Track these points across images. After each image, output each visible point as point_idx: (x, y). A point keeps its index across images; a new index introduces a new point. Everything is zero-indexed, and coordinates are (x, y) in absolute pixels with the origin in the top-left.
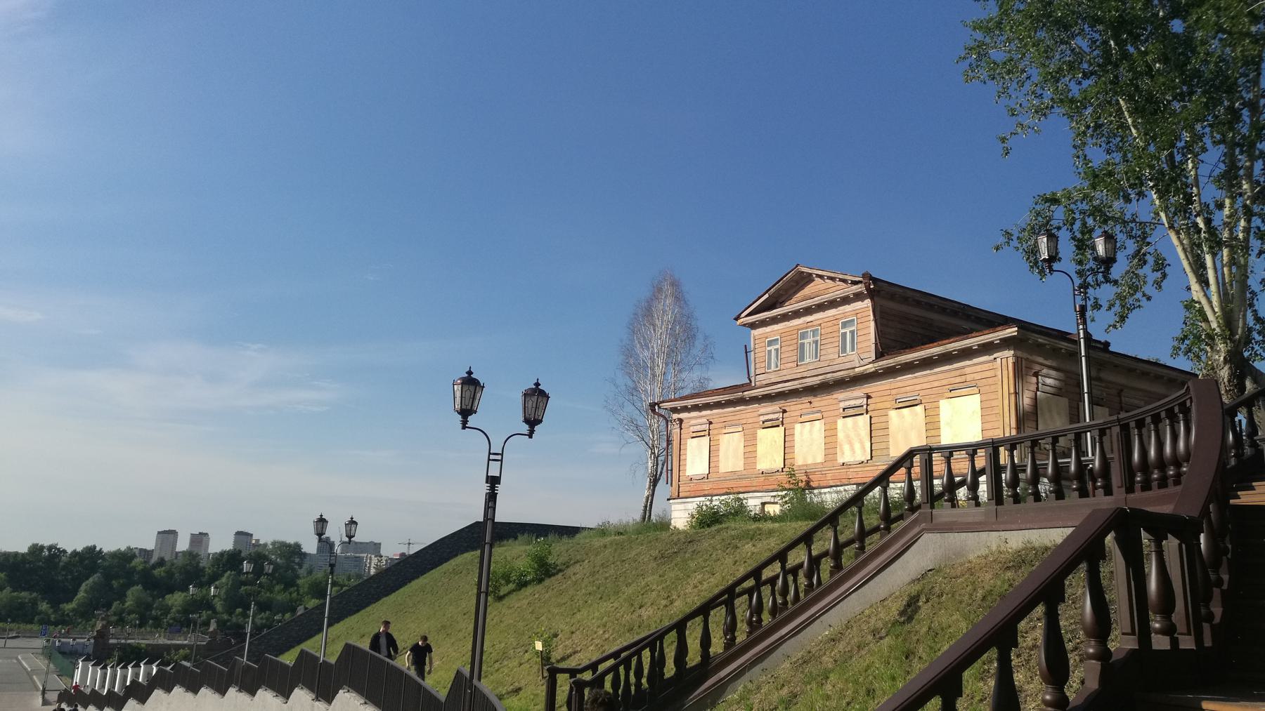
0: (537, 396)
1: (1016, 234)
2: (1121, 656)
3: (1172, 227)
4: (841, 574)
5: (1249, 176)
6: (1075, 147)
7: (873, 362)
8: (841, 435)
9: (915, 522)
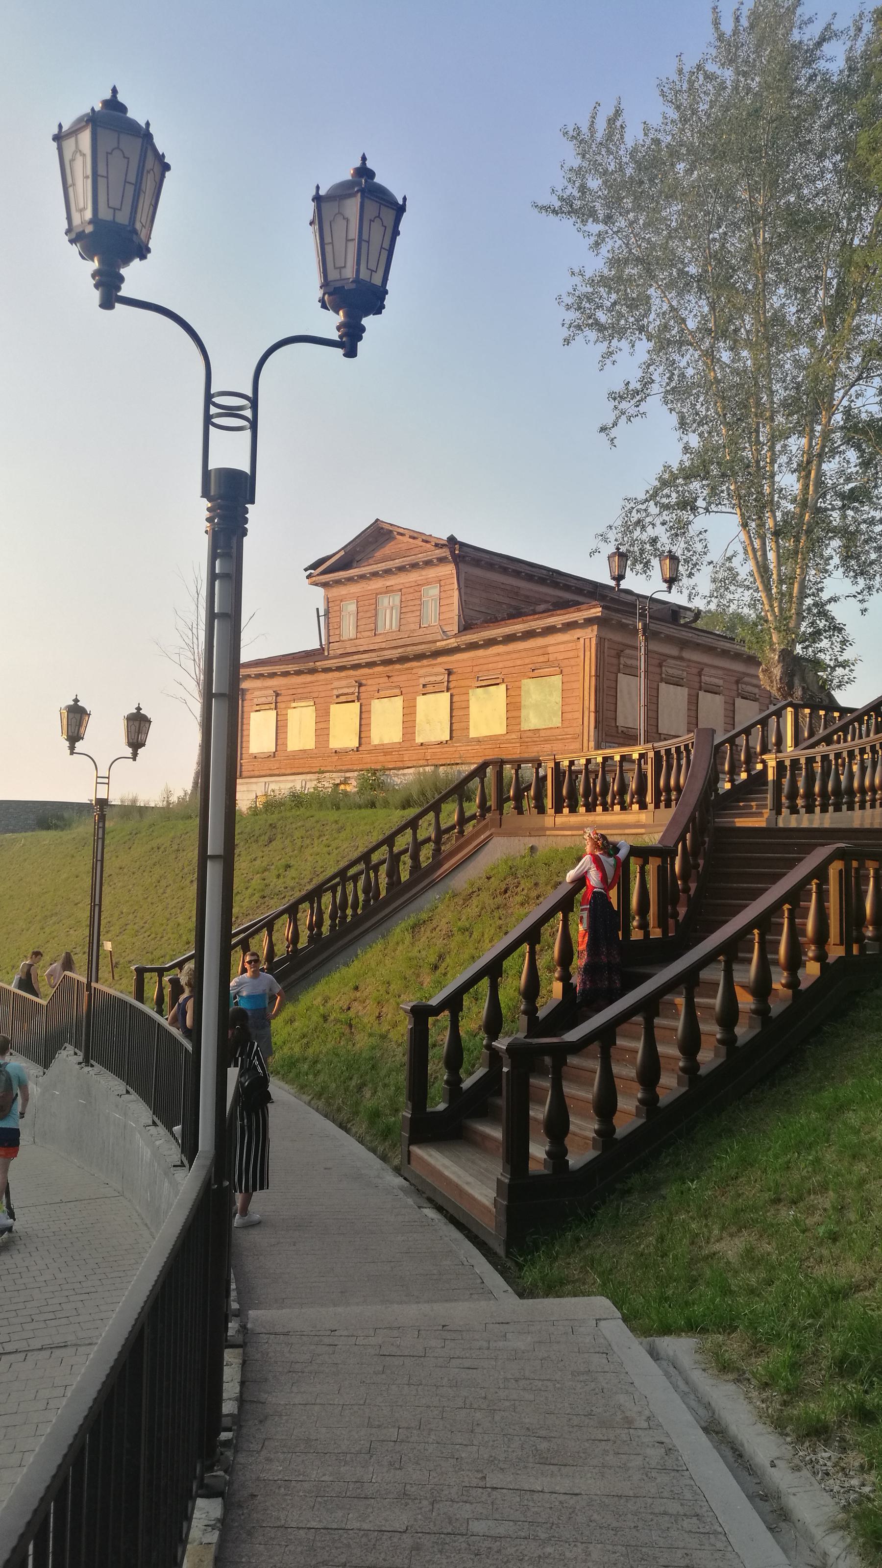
7: (455, 636)
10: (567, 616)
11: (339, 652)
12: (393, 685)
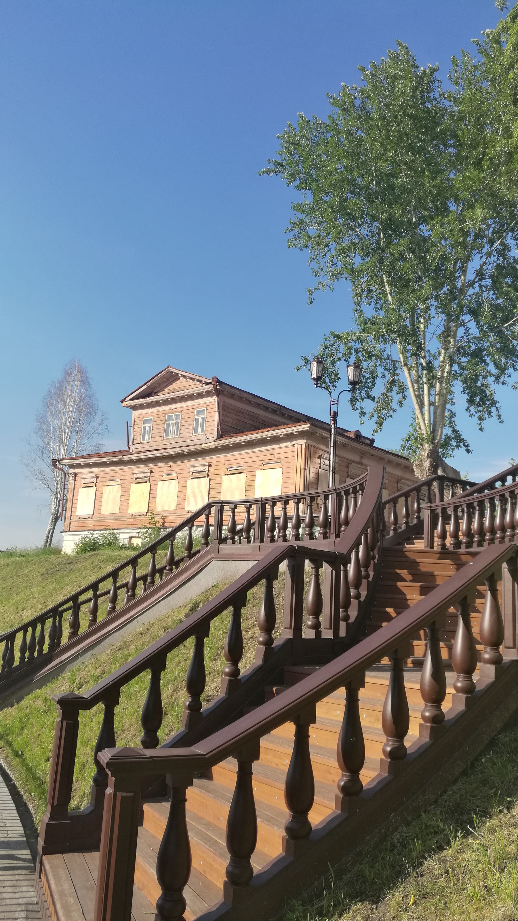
3: (406, 365)
4: (154, 588)
5: (454, 336)
8: (189, 491)
9: (208, 552)
10: (287, 429)
11: (139, 450)
12: (173, 472)
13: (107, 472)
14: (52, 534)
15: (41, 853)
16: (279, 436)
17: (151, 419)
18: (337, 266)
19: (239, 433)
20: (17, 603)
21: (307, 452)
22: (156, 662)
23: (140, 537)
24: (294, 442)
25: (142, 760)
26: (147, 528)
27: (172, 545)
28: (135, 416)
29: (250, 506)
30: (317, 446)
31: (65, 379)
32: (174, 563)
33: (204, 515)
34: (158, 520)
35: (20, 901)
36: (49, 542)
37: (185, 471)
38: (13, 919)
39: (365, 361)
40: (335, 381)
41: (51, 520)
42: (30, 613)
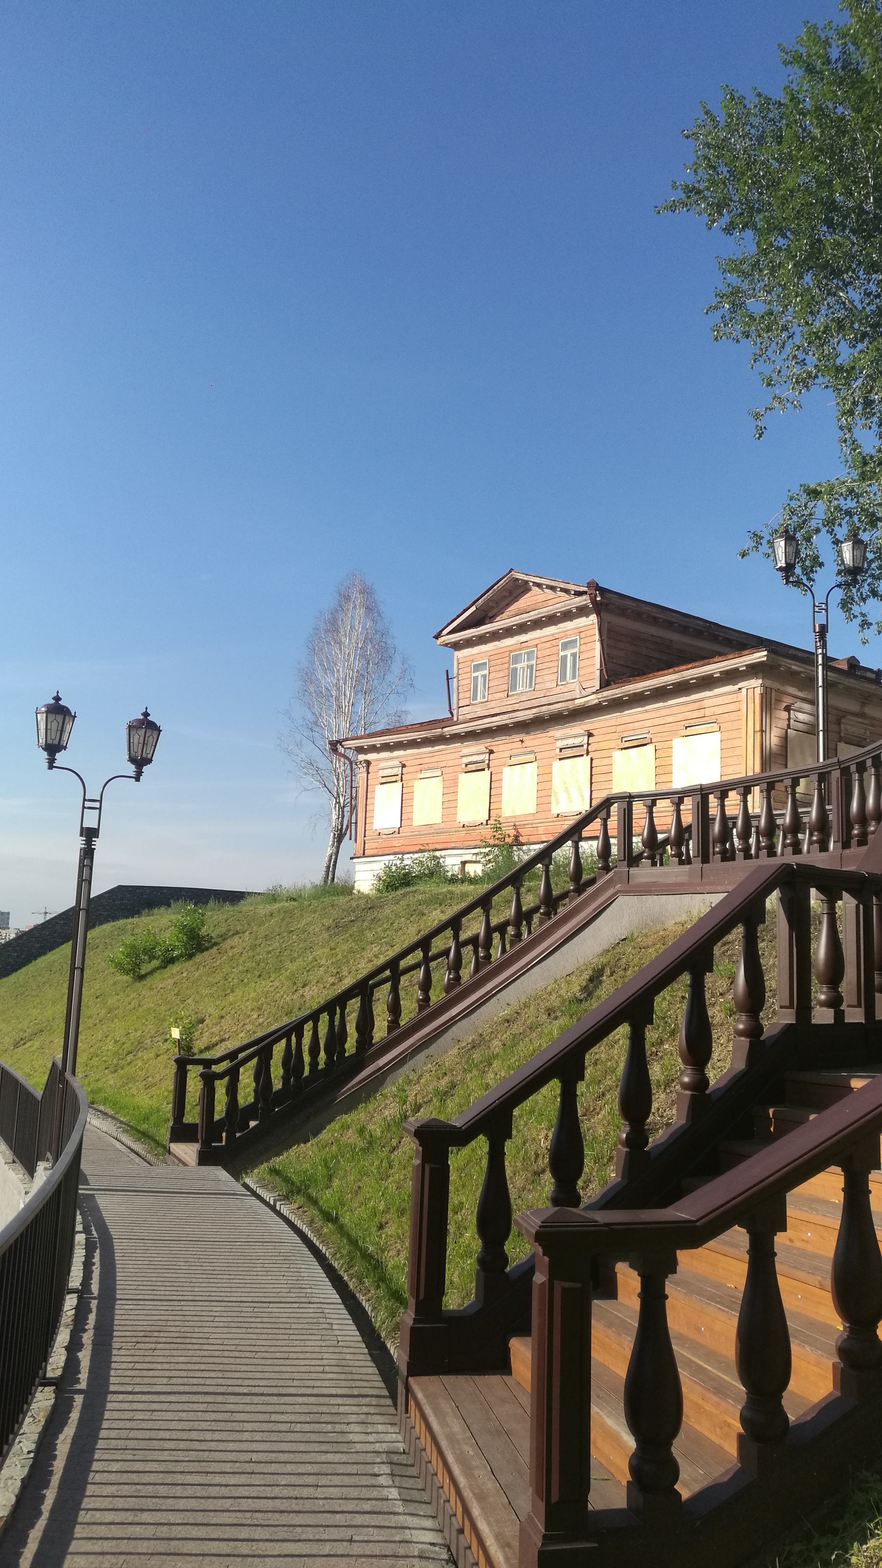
0: (145, 729)
1: (767, 537)
2: (776, 1031)
6: (841, 428)
9: (610, 882)
10: (726, 663)
11: (469, 717)
13: (418, 757)
14: (335, 862)
15: (406, 1374)
16: (712, 675)
17: (485, 663)
18: (805, 364)
19: (638, 675)
20: (293, 975)
21: (764, 700)
22: (567, 1066)
23: (479, 862)
24: (740, 685)
25: (641, 1226)
26: (489, 846)
27: (547, 871)
28: (458, 660)
29: (681, 801)
30: (782, 688)
31: (341, 606)
32: (550, 902)
33: (598, 820)
34: (507, 832)
35: (378, 1447)
36: (330, 876)
37: (548, 747)
38: (371, 1475)
39: (864, 531)
40: (812, 571)
41: (331, 839)
42: (316, 991)
